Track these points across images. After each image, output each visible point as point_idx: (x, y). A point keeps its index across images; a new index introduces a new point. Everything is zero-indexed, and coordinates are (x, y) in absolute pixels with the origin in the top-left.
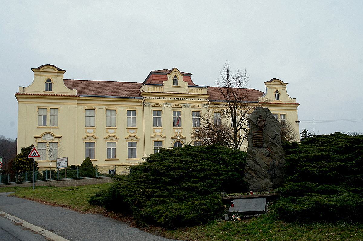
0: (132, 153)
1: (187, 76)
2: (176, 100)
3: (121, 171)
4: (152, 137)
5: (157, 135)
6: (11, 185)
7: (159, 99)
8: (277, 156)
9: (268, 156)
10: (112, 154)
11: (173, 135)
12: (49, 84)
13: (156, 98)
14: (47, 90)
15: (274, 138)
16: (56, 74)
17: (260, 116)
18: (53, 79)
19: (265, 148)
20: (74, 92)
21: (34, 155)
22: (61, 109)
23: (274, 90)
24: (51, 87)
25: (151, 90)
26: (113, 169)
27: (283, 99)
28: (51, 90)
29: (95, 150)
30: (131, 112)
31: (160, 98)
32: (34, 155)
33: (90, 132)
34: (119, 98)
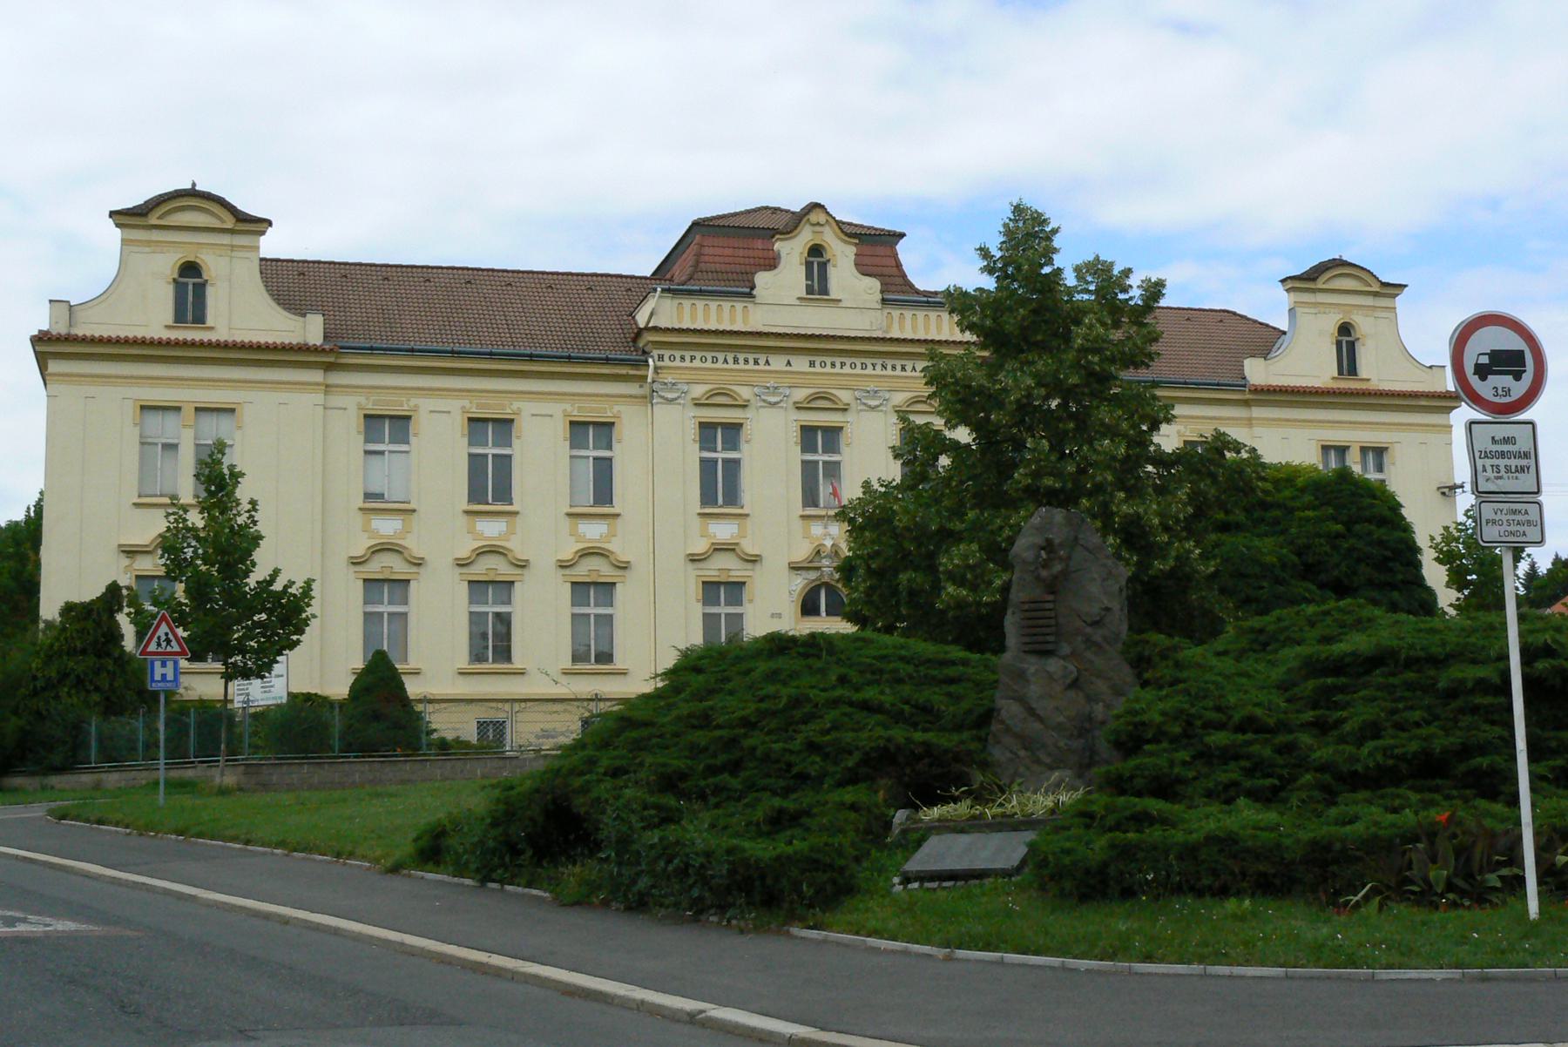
0: (595, 652)
2: (818, 369)
3: (537, 728)
4: (694, 559)
5: (719, 548)
7: (731, 365)
8: (1102, 686)
9: (1075, 684)
10: (493, 642)
11: (802, 552)
13: (715, 359)
14: (180, 317)
15: (1096, 624)
16: (226, 239)
17: (1049, 542)
18: (214, 265)
19: (1064, 658)
20: (311, 330)
22: (247, 414)
23: (1331, 322)
24: (195, 296)
25: (694, 318)
26: (501, 716)
27: (1375, 370)
28: (200, 319)
29: (412, 620)
30: (591, 432)
33: (387, 527)
34: (531, 358)
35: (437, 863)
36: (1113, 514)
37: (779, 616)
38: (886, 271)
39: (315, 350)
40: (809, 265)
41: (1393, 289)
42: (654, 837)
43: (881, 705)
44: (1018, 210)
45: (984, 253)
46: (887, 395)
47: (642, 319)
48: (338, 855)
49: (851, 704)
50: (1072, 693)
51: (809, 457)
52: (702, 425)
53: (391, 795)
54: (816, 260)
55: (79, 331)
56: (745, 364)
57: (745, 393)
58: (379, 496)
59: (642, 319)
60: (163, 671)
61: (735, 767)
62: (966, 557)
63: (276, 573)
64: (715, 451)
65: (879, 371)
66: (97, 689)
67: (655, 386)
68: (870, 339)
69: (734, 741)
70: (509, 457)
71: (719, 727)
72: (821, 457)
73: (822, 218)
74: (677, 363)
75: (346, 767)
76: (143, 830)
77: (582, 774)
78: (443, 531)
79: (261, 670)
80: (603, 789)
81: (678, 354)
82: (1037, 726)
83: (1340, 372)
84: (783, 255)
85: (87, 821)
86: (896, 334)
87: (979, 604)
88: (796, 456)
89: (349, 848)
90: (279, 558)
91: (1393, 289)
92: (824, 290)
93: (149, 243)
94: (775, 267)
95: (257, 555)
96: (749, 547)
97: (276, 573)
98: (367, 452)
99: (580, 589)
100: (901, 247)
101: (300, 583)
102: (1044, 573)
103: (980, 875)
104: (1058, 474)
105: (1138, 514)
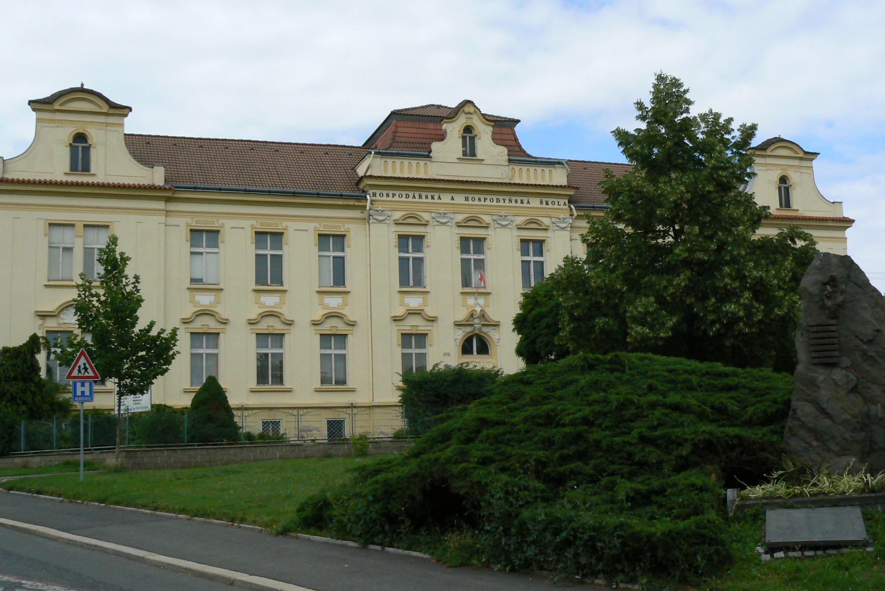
1: (504, 128)
2: (470, 202)
4: (396, 319)
5: (412, 313)
6: (50, 458)
7: (417, 200)
9: (854, 390)
10: (270, 371)
11: (462, 315)
12: (80, 149)
14: (74, 168)
15: (870, 342)
16: (102, 119)
18: (95, 135)
20: (157, 176)
21: (83, 371)
23: (775, 175)
28: (86, 168)
29: (221, 358)
30: (332, 241)
31: (420, 197)
32: (83, 371)
33: (205, 300)
34: (294, 194)
35: (320, 528)
36: (745, 276)
37: (449, 354)
38: (508, 143)
39: (159, 189)
40: (464, 138)
41: (811, 156)
42: (540, 512)
43: (689, 406)
44: (661, 78)
45: (640, 106)
46: (512, 218)
47: (361, 171)
48: (233, 520)
49: (665, 405)
50: (852, 396)
51: (465, 256)
52: (400, 237)
53: (235, 472)
54: (468, 135)
55: (9, 176)
56: (426, 199)
57: (426, 216)
58: (200, 281)
59: (361, 171)
60: (83, 389)
61: (582, 456)
62: (645, 306)
63: (152, 325)
64: (408, 252)
65: (507, 203)
66: (24, 403)
67: (371, 212)
68: (501, 184)
69: (579, 436)
70: (281, 256)
71: (564, 426)
72: (473, 257)
73: (472, 110)
74: (385, 198)
75: (192, 452)
76: (73, 498)
77: (457, 462)
78: (241, 305)
79: (141, 390)
80: (479, 474)
81: (385, 192)
82: (827, 422)
83: (781, 206)
84: (448, 131)
85: (29, 492)
86: (517, 181)
87: (657, 338)
88: (458, 256)
89: (240, 515)
90: (151, 316)
91: (811, 156)
92: (473, 154)
93: (53, 121)
94: (442, 140)
95: (139, 313)
96: (430, 312)
97: (152, 325)
98: (192, 253)
99: (325, 338)
100: (517, 128)
101: (169, 331)
102: (829, 303)
103: (837, 545)
104: (705, 250)
105: (761, 276)
